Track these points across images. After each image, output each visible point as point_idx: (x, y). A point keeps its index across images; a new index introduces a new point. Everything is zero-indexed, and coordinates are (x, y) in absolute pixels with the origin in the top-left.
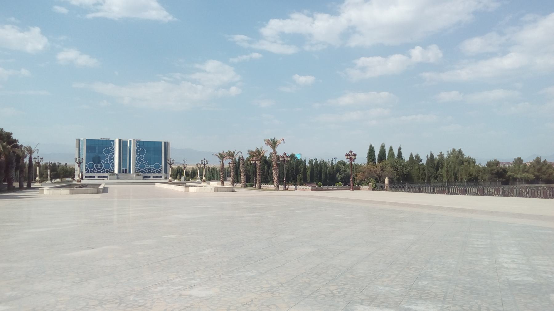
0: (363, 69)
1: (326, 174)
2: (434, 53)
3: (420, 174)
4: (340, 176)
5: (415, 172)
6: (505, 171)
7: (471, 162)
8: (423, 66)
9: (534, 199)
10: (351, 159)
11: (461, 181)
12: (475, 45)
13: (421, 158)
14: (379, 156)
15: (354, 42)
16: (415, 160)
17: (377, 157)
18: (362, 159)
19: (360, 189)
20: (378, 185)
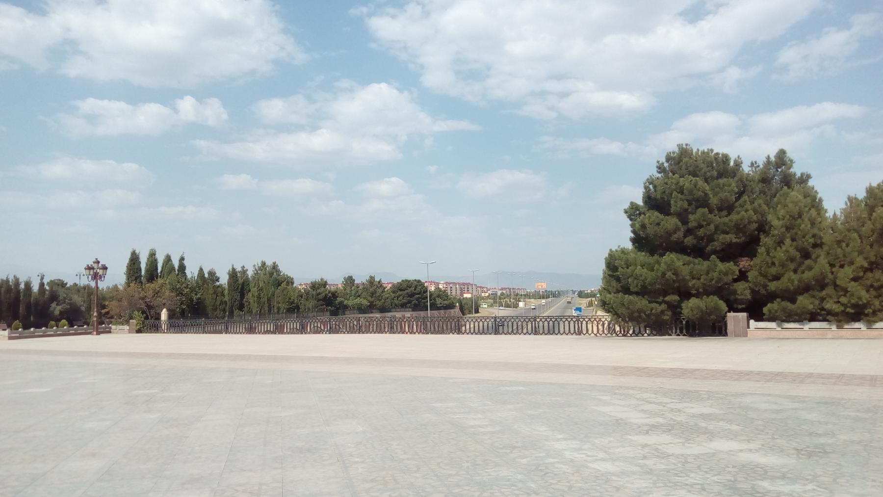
0: (92, 119)
1: (28, 307)
2: (214, 112)
3: (218, 303)
4: (59, 308)
5: (209, 301)
6: (334, 295)
7: (290, 281)
8: (197, 129)
9: (380, 335)
10: (96, 277)
11: (278, 312)
12: (274, 109)
13: (218, 275)
14: (147, 271)
15: (75, 69)
16: (208, 280)
17: (143, 272)
18: (116, 277)
19: (110, 332)
20: (149, 322)
